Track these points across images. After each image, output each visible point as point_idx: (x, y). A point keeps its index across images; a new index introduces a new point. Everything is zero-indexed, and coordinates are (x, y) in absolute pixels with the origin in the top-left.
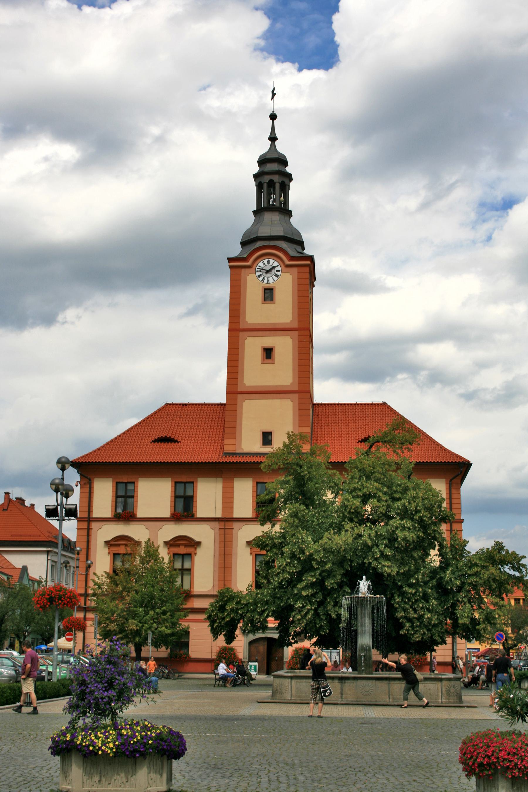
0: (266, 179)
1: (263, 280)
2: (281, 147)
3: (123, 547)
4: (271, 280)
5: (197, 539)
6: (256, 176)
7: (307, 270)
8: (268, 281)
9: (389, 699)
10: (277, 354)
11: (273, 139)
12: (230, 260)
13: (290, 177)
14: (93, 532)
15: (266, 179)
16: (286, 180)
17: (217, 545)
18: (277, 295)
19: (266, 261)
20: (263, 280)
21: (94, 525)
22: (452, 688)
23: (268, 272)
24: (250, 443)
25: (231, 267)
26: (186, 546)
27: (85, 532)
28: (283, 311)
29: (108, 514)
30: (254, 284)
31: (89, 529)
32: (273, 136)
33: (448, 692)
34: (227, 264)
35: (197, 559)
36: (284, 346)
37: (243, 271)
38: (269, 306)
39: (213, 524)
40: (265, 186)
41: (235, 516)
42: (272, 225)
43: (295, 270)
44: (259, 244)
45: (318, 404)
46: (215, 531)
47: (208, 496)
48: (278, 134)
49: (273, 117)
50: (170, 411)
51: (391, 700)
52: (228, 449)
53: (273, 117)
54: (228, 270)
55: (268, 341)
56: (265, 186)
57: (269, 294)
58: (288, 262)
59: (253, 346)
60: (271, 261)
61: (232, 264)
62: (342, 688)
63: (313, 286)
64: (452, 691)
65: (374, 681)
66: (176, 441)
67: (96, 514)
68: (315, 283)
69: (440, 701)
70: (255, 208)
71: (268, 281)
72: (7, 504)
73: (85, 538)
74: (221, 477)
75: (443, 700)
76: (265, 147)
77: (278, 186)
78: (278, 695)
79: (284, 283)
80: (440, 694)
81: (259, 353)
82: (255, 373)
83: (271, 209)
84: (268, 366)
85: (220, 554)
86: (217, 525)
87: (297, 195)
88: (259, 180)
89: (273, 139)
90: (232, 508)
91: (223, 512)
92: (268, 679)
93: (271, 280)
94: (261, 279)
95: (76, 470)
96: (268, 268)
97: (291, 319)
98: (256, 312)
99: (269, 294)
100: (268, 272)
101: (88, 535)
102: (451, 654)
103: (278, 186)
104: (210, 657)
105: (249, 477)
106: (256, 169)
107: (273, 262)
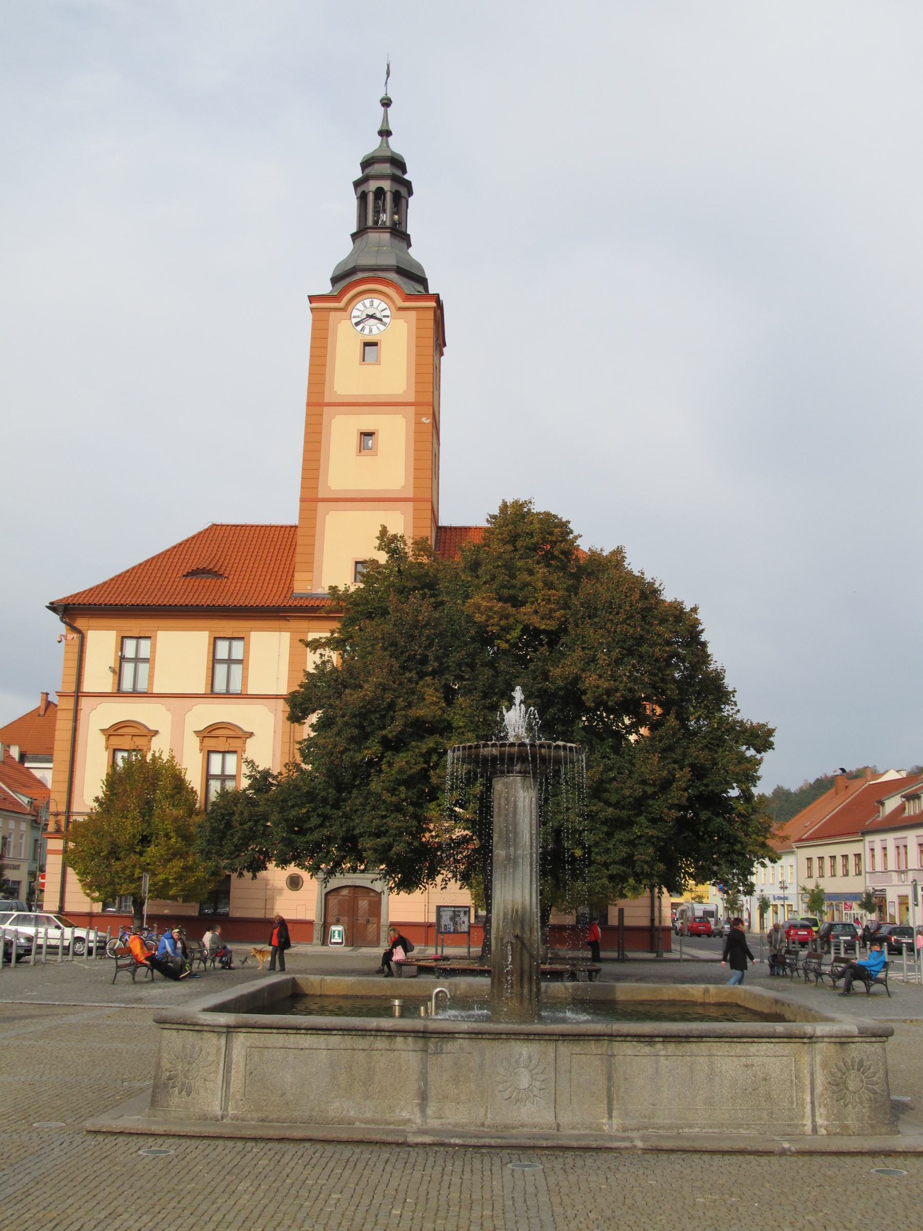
0: (373, 185)
1: (363, 329)
2: (396, 145)
4: (373, 330)
5: (247, 729)
6: (357, 184)
7: (431, 315)
8: (371, 331)
9: (610, 1117)
10: (382, 438)
11: (385, 133)
12: (312, 299)
13: (408, 185)
14: (82, 716)
15: (373, 185)
16: (404, 192)
17: (279, 738)
19: (367, 302)
20: (363, 329)
21: (85, 702)
22: (853, 1073)
25: (312, 309)
28: (394, 374)
30: (346, 337)
32: (385, 128)
33: (838, 1086)
34: (307, 304)
36: (395, 431)
37: (332, 314)
40: (371, 198)
43: (413, 314)
44: (360, 275)
45: (445, 528)
46: (275, 715)
49: (386, 103)
50: (217, 534)
51: (616, 1121)
53: (386, 103)
54: (309, 316)
55: (367, 422)
56: (371, 198)
59: (342, 430)
60: (376, 302)
61: (315, 305)
62: (424, 1075)
63: (442, 354)
64: (852, 1085)
66: (217, 574)
67: (87, 687)
68: (445, 350)
69: (808, 1122)
70: (354, 230)
71: (371, 331)
72: (43, 708)
75: (820, 1121)
77: (389, 197)
78: (176, 1098)
79: (397, 332)
80: (808, 1099)
81: (355, 439)
82: (344, 471)
84: (366, 460)
85: (282, 753)
87: (418, 216)
88: (360, 190)
89: (385, 133)
92: (354, 954)
93: (375, 331)
94: (359, 328)
97: (405, 388)
98: (349, 377)
102: (648, 914)
103: (389, 197)
104: (262, 916)
105: (280, 630)
106: (358, 174)
107: (379, 305)
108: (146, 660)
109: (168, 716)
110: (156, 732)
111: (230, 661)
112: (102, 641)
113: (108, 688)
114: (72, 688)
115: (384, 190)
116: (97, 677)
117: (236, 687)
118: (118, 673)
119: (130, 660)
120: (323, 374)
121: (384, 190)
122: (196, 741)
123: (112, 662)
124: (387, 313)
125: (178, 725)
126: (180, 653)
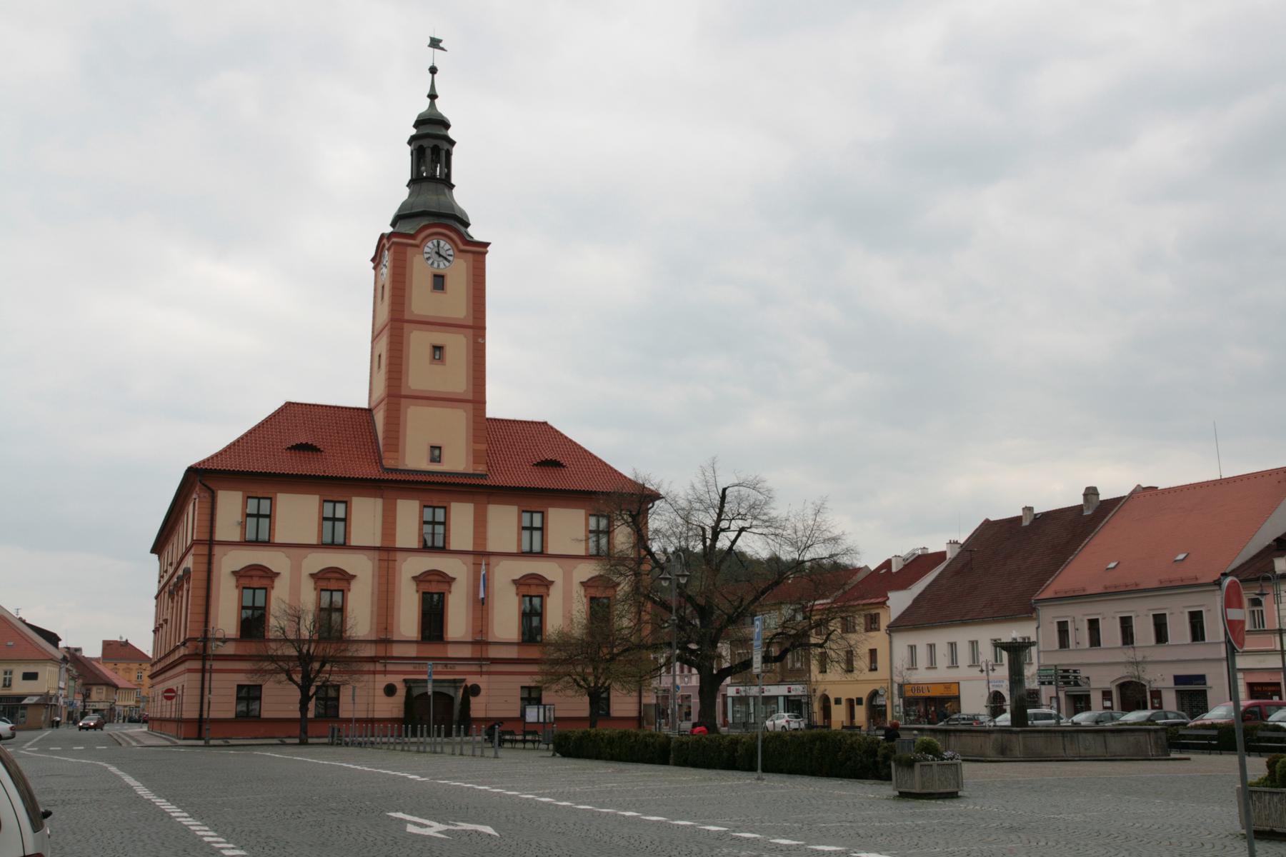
2: (442, 107)
3: (256, 579)
10: (449, 353)
11: (433, 96)
18: (449, 282)
21: (218, 550)
23: (438, 253)
24: (415, 458)
26: (337, 579)
27: (205, 560)
29: (415, 544)
31: (210, 556)
35: (352, 598)
36: (456, 344)
37: (409, 249)
38: (438, 295)
39: (371, 553)
41: (398, 545)
42: (430, 200)
43: (470, 256)
47: (365, 517)
48: (438, 91)
49: (433, 70)
52: (388, 463)
53: (433, 70)
55: (439, 337)
57: (439, 281)
58: (462, 247)
59: (418, 342)
65: (1238, 774)
67: (219, 536)
73: (204, 567)
74: (382, 497)
76: (423, 106)
77: (428, 152)
81: (427, 352)
82: (420, 375)
83: (432, 178)
84: (438, 368)
86: (376, 554)
89: (433, 96)
90: (394, 535)
91: (383, 540)
93: (442, 266)
95: (992, 519)
96: (442, 252)
98: (422, 301)
99: (439, 281)
100: (438, 253)
101: (210, 563)
105: (375, 497)
108: (524, 528)
109: (560, 572)
110: (278, 574)
111: (258, 516)
112: (230, 504)
113: (236, 537)
114: (206, 537)
115: (431, 144)
116: (227, 527)
117: (264, 536)
118: (243, 525)
119: (537, 529)
120: (403, 296)
121: (431, 144)
122: (413, 586)
123: (239, 518)
124: (451, 252)
125: (296, 569)
126: (297, 515)
